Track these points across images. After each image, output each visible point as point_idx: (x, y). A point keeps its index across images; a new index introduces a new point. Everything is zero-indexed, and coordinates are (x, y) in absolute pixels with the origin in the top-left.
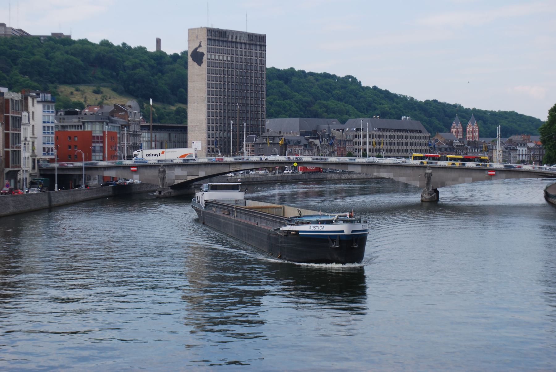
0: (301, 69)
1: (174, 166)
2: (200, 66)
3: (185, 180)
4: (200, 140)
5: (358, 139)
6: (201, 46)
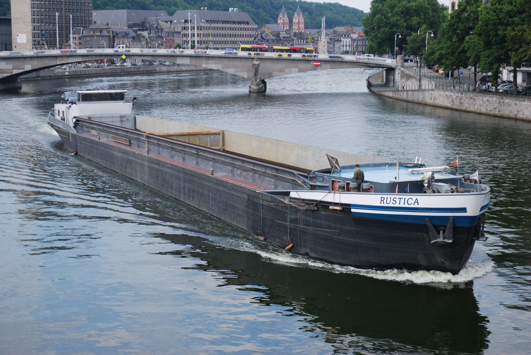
3: (11, 74)
4: (25, 33)
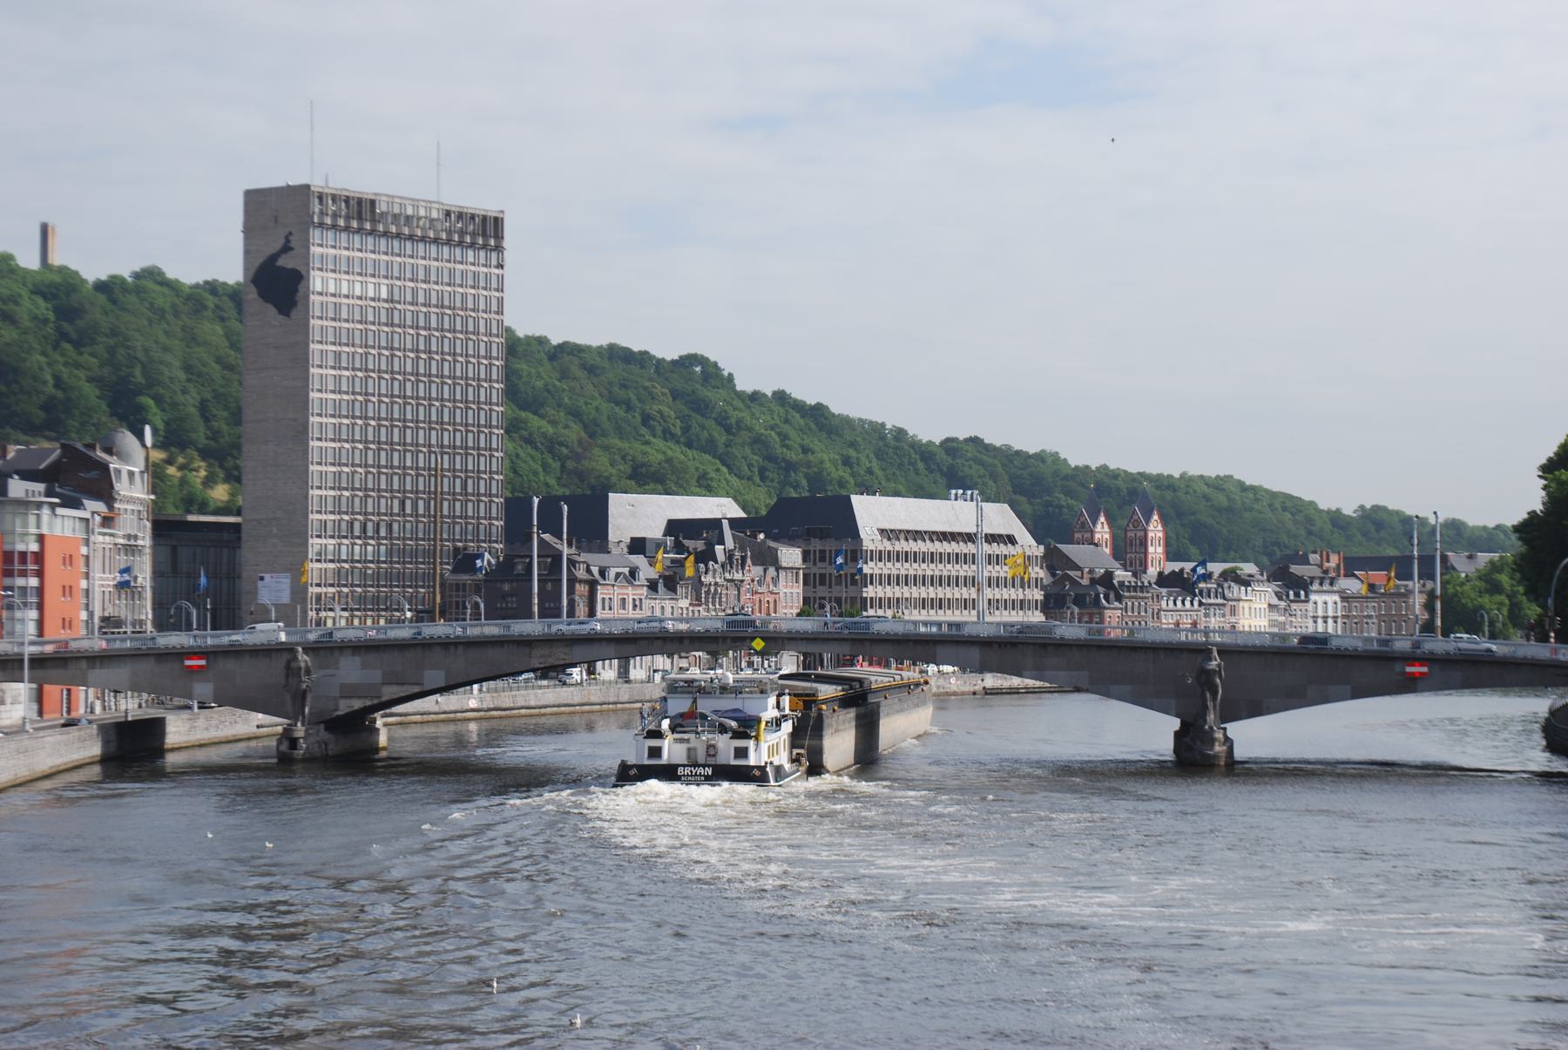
0: (536, 331)
2: (289, 317)
4: (286, 570)
5: (815, 564)
6: (291, 249)
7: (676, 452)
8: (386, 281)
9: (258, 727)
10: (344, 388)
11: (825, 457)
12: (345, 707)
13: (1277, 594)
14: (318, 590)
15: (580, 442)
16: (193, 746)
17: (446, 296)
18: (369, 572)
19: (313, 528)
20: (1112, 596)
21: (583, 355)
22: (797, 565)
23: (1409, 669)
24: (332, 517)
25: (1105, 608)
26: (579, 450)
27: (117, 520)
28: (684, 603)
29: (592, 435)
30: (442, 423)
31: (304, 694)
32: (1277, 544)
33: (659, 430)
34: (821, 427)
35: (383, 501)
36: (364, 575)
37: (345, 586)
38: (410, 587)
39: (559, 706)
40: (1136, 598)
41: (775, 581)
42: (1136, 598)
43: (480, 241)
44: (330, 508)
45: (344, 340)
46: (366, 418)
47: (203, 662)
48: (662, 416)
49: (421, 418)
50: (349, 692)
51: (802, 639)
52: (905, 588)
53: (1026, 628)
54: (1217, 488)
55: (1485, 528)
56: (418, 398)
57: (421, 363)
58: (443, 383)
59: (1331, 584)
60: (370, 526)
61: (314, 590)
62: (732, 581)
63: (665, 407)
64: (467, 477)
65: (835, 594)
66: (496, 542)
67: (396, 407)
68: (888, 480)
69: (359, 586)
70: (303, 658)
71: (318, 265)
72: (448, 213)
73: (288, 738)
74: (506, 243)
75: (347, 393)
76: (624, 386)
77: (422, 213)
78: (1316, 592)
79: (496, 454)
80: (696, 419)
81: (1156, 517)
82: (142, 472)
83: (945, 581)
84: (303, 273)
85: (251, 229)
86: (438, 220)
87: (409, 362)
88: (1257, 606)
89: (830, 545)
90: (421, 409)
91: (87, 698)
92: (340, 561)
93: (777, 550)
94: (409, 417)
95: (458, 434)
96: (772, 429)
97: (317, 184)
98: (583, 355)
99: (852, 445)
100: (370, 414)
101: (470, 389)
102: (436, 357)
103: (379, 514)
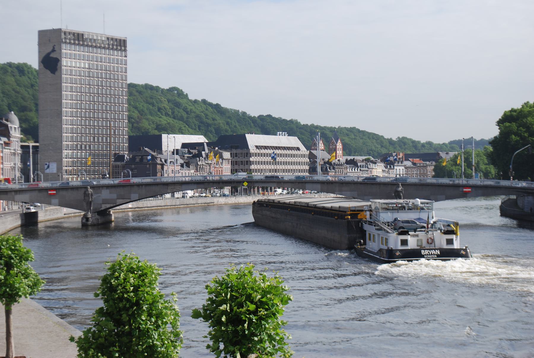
1: (101, 189)
6: (55, 51)
7: (170, 120)
8: (87, 62)
9: (64, 214)
10: (74, 99)
11: (221, 122)
12: (104, 207)
13: (385, 166)
14: (66, 168)
15: (138, 117)
16: (46, 221)
17: (108, 67)
18: (83, 162)
19: (64, 147)
20: (331, 168)
21: (137, 87)
22: (229, 158)
23: (465, 190)
24: (70, 143)
25: (329, 172)
26: (138, 120)
27: (11, 144)
28: (192, 171)
29: (142, 115)
30: (107, 111)
31: (91, 202)
32: (371, 150)
33: (164, 113)
34: (219, 112)
35: (87, 137)
36: (81, 163)
37: (75, 167)
38: (97, 167)
39: (157, 207)
40: (339, 168)
41: (222, 163)
42: (339, 168)
43: (119, 48)
44: (70, 140)
45: (74, 82)
46: (81, 109)
47: (55, 192)
48: (165, 108)
49: (100, 109)
50: (105, 201)
51: (260, 182)
52: (264, 166)
53: (304, 177)
54: (351, 132)
55: (439, 144)
56: (99, 102)
57: (100, 90)
58: (107, 97)
59: (402, 163)
60: (83, 146)
61: (65, 168)
62: (208, 164)
63: (165, 105)
64: (115, 129)
65: (241, 168)
66: (126, 151)
67: (91, 105)
68: (242, 129)
69: (80, 167)
70: (90, 190)
71: (64, 56)
72: (108, 39)
73: (85, 217)
74: (128, 48)
75: (75, 100)
76: (151, 98)
77: (99, 38)
78: (397, 166)
79: (125, 121)
80: (176, 109)
81: (339, 141)
82: (18, 128)
83: (263, 163)
84: (59, 59)
85: (41, 44)
86: (105, 41)
87: (95, 89)
88: (379, 171)
89: (239, 151)
90: (100, 106)
91: (3, 205)
92: (73, 158)
93: (222, 153)
94: (96, 108)
95: (112, 114)
96: (202, 112)
97: (64, 28)
98: (137, 87)
99: (229, 117)
100: (83, 108)
101: (116, 99)
102: (105, 88)
103: (86, 142)
